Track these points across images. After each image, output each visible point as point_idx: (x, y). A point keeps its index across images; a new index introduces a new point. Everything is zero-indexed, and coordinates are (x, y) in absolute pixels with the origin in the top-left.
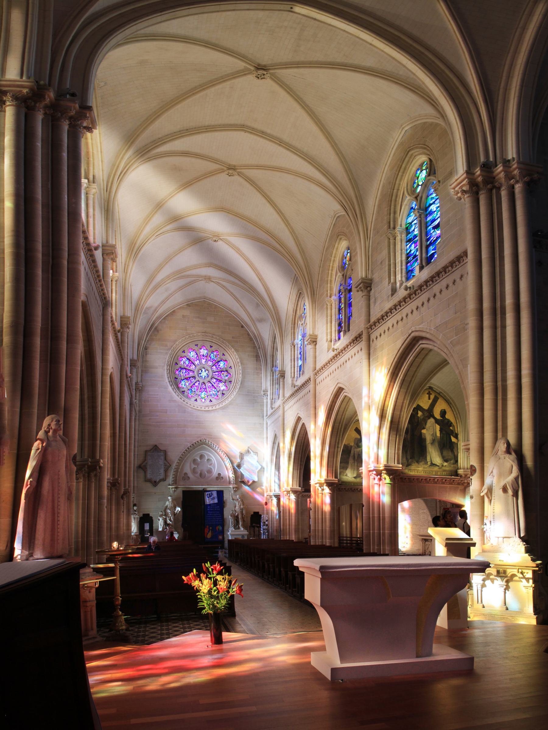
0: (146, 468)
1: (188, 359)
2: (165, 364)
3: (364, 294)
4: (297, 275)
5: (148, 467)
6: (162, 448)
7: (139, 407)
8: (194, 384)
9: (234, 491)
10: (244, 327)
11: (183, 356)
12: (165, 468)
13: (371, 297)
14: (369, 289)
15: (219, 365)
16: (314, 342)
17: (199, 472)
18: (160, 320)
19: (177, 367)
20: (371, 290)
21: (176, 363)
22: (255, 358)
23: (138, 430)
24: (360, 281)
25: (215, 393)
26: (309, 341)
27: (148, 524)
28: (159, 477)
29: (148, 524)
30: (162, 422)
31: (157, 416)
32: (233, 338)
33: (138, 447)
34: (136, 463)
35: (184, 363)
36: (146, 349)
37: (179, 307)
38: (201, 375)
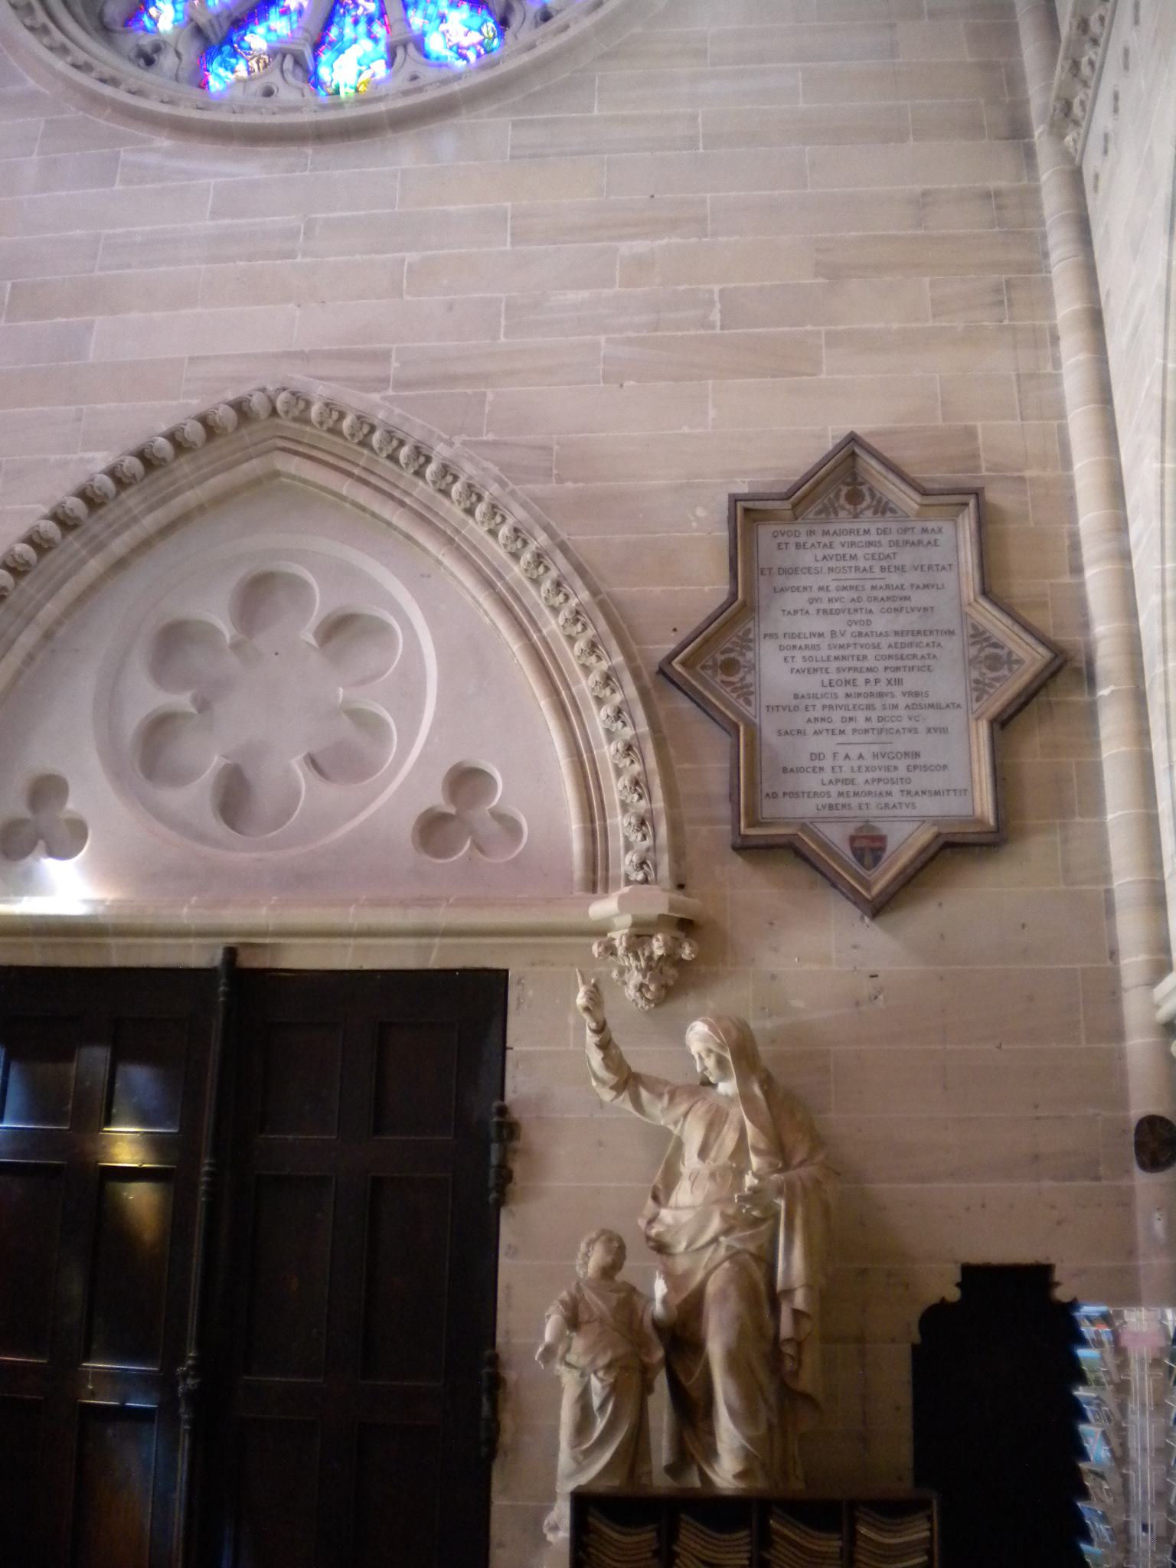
9: (653, 967)
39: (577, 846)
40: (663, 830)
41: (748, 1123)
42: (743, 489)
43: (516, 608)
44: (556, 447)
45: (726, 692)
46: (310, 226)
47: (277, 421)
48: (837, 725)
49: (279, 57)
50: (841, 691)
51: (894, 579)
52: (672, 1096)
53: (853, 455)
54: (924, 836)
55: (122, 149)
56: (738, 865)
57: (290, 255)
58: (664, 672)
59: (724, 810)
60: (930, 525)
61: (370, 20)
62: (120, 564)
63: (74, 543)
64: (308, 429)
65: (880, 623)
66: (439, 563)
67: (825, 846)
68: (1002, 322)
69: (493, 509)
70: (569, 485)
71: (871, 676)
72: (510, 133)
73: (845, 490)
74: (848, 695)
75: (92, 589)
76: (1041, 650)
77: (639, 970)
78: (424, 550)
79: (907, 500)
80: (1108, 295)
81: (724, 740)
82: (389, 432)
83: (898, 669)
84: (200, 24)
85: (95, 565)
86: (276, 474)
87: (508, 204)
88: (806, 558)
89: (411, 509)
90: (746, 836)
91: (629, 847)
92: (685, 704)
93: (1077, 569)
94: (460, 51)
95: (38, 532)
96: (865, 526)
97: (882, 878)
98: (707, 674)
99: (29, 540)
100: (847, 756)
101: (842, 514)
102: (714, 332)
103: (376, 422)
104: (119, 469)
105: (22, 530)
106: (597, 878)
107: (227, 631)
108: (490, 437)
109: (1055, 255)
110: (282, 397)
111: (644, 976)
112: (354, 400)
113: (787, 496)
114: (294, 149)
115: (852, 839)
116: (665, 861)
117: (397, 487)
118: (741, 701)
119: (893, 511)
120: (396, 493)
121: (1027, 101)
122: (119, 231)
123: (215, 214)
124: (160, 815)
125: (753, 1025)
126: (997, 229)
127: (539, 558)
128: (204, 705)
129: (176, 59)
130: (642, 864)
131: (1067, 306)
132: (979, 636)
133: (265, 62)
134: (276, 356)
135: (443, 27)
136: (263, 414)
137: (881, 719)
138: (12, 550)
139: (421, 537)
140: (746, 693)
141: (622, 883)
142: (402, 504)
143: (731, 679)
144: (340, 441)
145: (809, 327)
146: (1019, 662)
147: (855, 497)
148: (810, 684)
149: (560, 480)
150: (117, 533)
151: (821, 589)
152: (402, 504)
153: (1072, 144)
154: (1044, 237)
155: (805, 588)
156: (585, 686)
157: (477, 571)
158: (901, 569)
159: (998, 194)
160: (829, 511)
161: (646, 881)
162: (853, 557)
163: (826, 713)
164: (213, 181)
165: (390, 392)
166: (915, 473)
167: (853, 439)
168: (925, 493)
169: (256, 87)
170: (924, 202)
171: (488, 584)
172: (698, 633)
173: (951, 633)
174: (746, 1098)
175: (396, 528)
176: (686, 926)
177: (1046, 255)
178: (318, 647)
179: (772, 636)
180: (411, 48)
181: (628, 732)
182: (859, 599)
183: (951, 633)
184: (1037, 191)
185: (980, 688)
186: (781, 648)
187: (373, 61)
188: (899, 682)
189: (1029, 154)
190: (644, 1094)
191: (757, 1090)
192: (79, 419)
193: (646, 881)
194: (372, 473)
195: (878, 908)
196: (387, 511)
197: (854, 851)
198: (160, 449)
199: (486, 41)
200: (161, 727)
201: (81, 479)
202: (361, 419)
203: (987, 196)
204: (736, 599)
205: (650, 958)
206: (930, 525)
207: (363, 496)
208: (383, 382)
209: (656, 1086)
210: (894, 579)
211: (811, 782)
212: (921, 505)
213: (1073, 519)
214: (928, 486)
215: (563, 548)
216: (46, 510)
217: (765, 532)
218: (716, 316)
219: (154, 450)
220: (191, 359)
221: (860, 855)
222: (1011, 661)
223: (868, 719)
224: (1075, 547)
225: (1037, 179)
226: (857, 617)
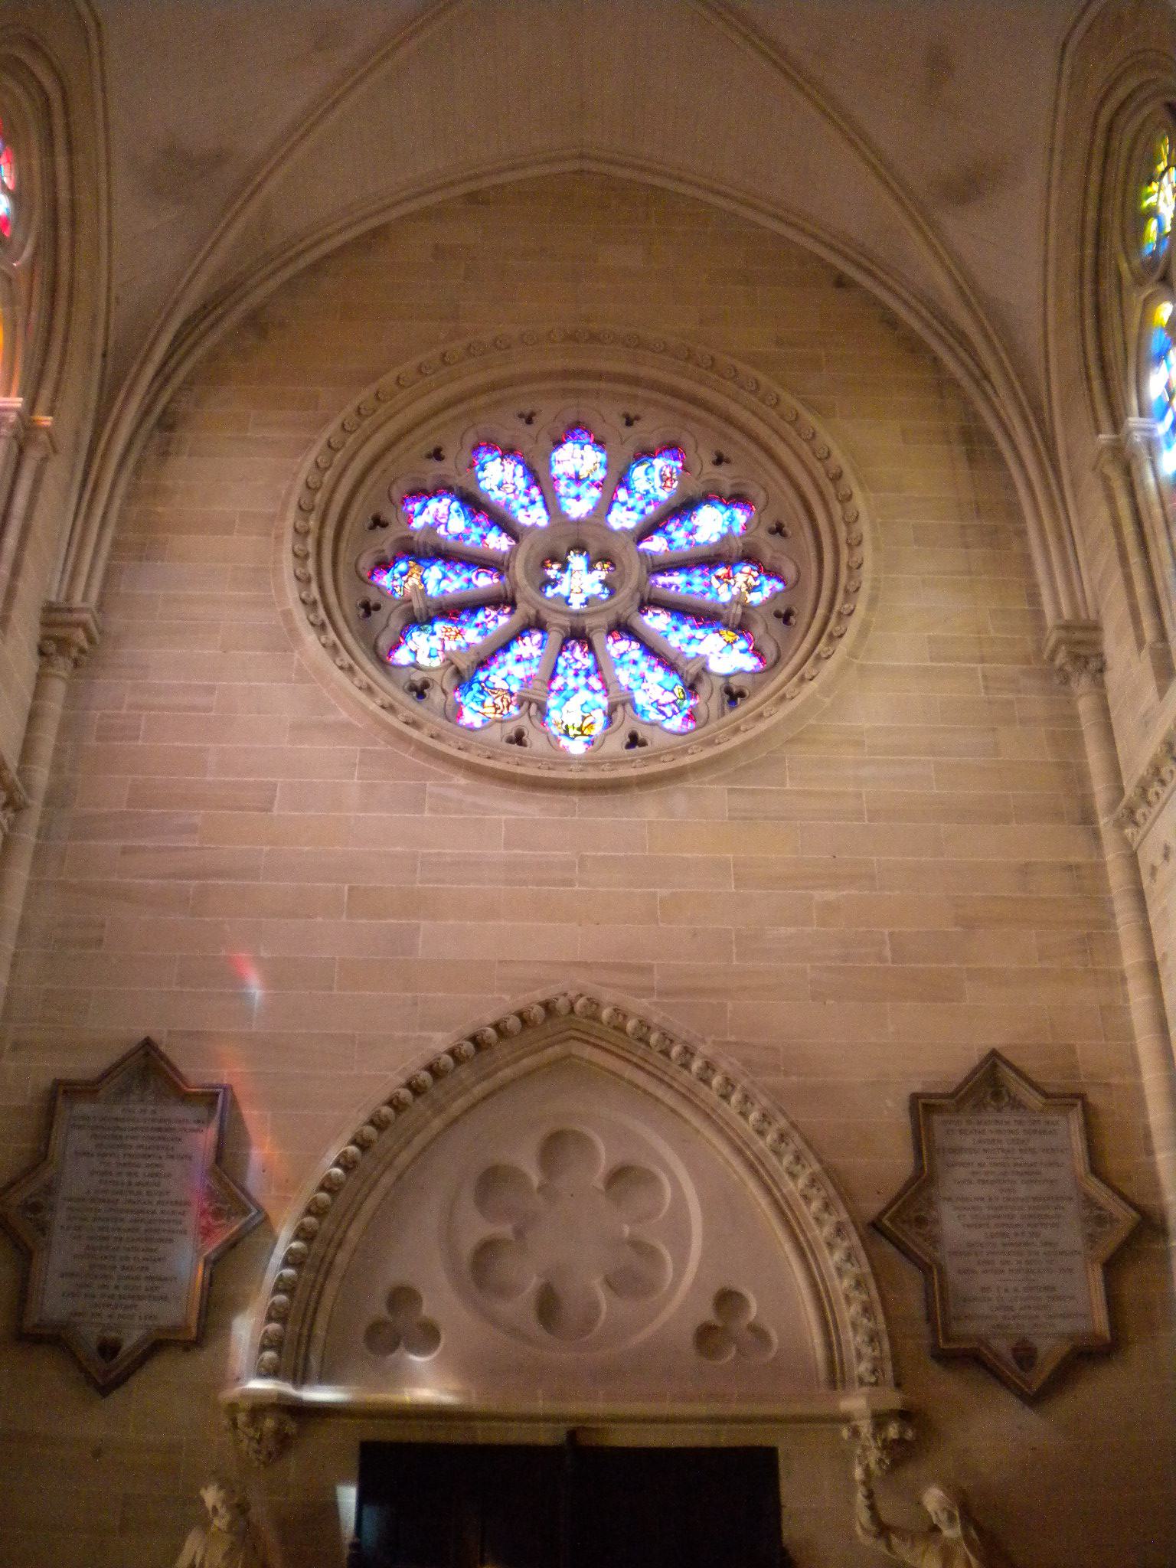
0: (43, 1228)
2: (285, 505)
5: (61, 1217)
6: (196, 1073)
7: (57, 767)
9: (888, 1446)
11: (429, 485)
17: (533, 1283)
19: (385, 542)
22: (959, 449)
30: (219, 874)
31: (193, 829)
32: (779, 343)
36: (171, 428)
37: (413, 206)
38: (562, 589)
39: (820, 1353)
40: (886, 1346)
41: (972, 1559)
42: (918, 1088)
43: (762, 1172)
44: (782, 1050)
45: (919, 1240)
46: (582, 859)
47: (573, 1017)
48: (998, 1266)
49: (526, 705)
50: (998, 1241)
51: (1028, 1158)
52: (913, 1538)
53: (995, 1066)
54: (1065, 1348)
55: (428, 783)
56: (935, 1369)
57: (569, 883)
58: (875, 1226)
59: (924, 1329)
60: (1049, 1118)
61: (588, 676)
62: (455, 1121)
63: (421, 1105)
64: (597, 1025)
65: (1022, 1191)
66: (698, 1131)
67: (996, 1356)
68: (1086, 966)
69: (746, 1098)
70: (794, 1079)
71: (1019, 1230)
72: (727, 798)
73: (990, 1090)
74: (1004, 1245)
75: (434, 1139)
76: (1134, 1214)
77: (878, 1448)
78: (686, 1121)
79: (1035, 1100)
80: (1165, 955)
81: (918, 1274)
82: (664, 1034)
83: (1036, 1226)
84: (460, 669)
85: (437, 1124)
86: (570, 1056)
87: (730, 855)
88: (968, 1141)
89: (677, 1091)
90: (943, 1349)
91: (860, 1356)
92: (891, 1249)
93: (1150, 1152)
94: (659, 707)
95: (398, 1098)
96: (1007, 1118)
97: (1038, 1378)
98: (906, 1227)
99: (390, 1103)
100: (1006, 1290)
101: (989, 1109)
102: (887, 965)
103: (652, 1025)
104: (458, 1050)
105: (385, 1095)
106: (836, 1377)
107: (535, 1178)
108: (732, 1038)
109: (1120, 920)
110: (582, 1001)
111: (882, 1454)
112: (639, 1005)
113: (951, 1096)
114: (563, 796)
115: (1015, 1350)
116: (888, 1367)
117: (666, 1073)
118: (931, 1248)
119: (1025, 1108)
120: (666, 1078)
121: (1093, 795)
122: (432, 851)
123: (508, 845)
124: (493, 1321)
125: (965, 1486)
126: (1079, 895)
127: (782, 1137)
128: (519, 1233)
129: (444, 697)
130: (874, 1371)
131: (1131, 958)
132: (1089, 1201)
133: (507, 701)
134: (565, 964)
135: (645, 686)
136: (564, 1011)
137: (1028, 1262)
138: (379, 1111)
139: (686, 1112)
140: (935, 1241)
141: (857, 1384)
142: (671, 1087)
143: (921, 1231)
144: (622, 1036)
145: (955, 965)
146: (1117, 1220)
147: (997, 1095)
148: (977, 1235)
149: (786, 1074)
150: (454, 1099)
151: (980, 1165)
152: (671, 1087)
153: (1130, 835)
154: (1111, 901)
155: (969, 1164)
156: (821, 1234)
157: (730, 1141)
158: (1033, 1151)
159: (1078, 867)
160: (979, 1106)
161: (876, 1384)
162: (1000, 1141)
163: (990, 1258)
164: (504, 817)
165: (655, 999)
166: (1034, 1078)
167: (994, 1054)
168: (1046, 1095)
169: (510, 729)
170: (1025, 870)
171: (739, 1152)
172: (899, 1196)
173: (1071, 1199)
174: (966, 1537)
175: (663, 1103)
176: (905, 1415)
177: (1113, 915)
178: (604, 1190)
179: (949, 1199)
180: (628, 707)
181: (855, 1270)
182: (1004, 1174)
183: (1071, 1199)
184: (1103, 865)
185: (1092, 1239)
186: (956, 1208)
187: (594, 710)
188: (1038, 1235)
189: (1096, 835)
190: (895, 1540)
191: (973, 1533)
192: (416, 1004)
193: (876, 1384)
194: (646, 1061)
195: (1034, 1400)
196: (660, 1092)
197: (1015, 1357)
198: (489, 1037)
199: (678, 701)
200: (487, 1249)
201: (429, 1058)
202: (641, 1023)
203: (1069, 868)
204: (922, 1174)
205: (884, 1440)
206: (1049, 1118)
207: (640, 1078)
208: (649, 991)
209: (904, 1533)
210: (1028, 1158)
211: (984, 1309)
212: (1045, 1104)
213: (1146, 1117)
214: (1049, 1090)
215: (794, 1126)
216: (403, 1080)
217: (937, 1119)
218: (888, 953)
219: (485, 1038)
220: (500, 962)
221: (1019, 1362)
222: (1112, 1220)
223: (1019, 1262)
224: (1148, 1136)
225: (1103, 857)
226: (1005, 1186)
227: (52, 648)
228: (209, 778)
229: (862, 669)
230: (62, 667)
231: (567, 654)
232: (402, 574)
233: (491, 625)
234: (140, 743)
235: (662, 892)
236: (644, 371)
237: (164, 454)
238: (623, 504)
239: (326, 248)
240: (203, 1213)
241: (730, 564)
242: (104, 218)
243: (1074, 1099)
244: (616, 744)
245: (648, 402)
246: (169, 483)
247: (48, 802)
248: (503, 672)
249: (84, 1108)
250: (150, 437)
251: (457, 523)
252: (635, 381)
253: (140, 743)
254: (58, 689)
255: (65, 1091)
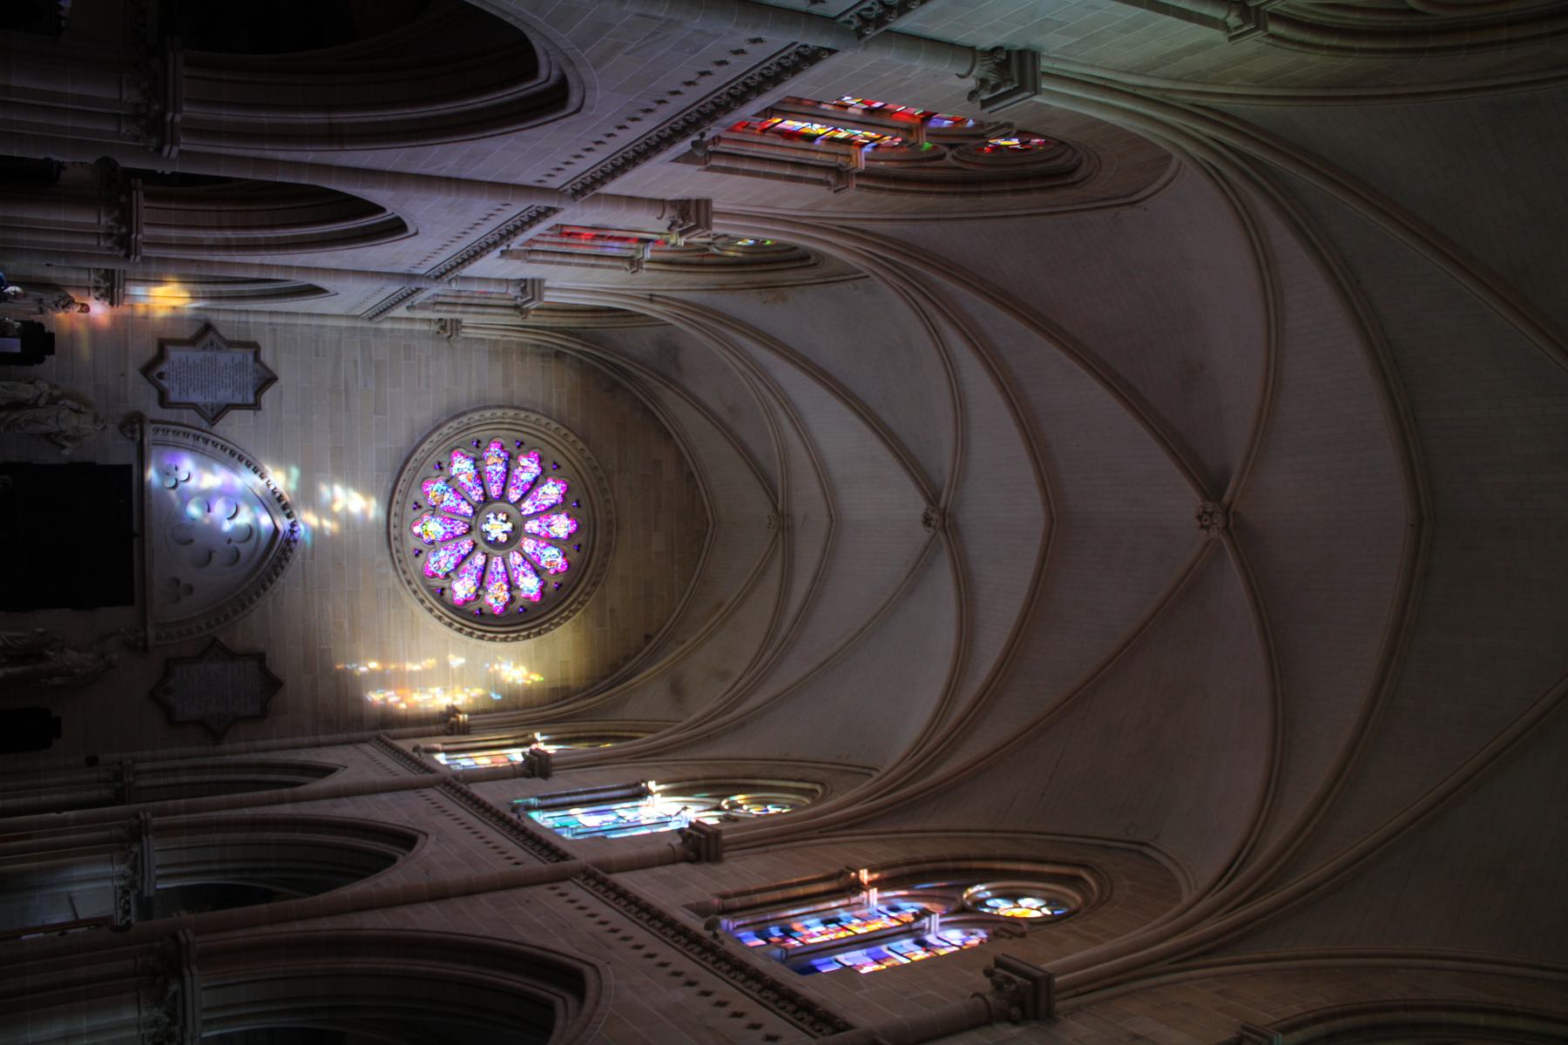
0: (204, 348)
1: (536, 479)
3: (990, 998)
4: (876, 775)
5: (209, 354)
8: (463, 499)
10: (647, 643)
12: (205, 406)
13: (988, 1029)
14: (1015, 1011)
15: (525, 575)
16: (697, 851)
18: (641, 397)
20: (1015, 1023)
21: (522, 443)
23: (321, 327)
24: (1039, 974)
25: (442, 566)
26: (695, 833)
27: (18, 349)
28: (177, 387)
29: (18, 349)
33: (271, 324)
34: (222, 317)
35: (524, 467)
37: (683, 449)
38: (492, 521)
131: (322, 738)
227: (443, 323)
228: (388, 390)
229: (447, 641)
230: (513, 291)
231: (461, 524)
232: (499, 455)
233: (474, 493)
234: (237, 424)
235: (345, 563)
236: (596, 553)
237: (543, 355)
238: (538, 545)
239: (657, 414)
240: (212, 404)
241: (509, 590)
242: (1084, 206)
243: (263, 714)
244: (418, 544)
245: (585, 553)
246: (528, 359)
247: (376, 329)
248: (451, 498)
249: (251, 357)
250: (551, 349)
251: (527, 477)
252: (593, 550)
253: (237, 424)
254: (425, 327)
255: (255, 347)
